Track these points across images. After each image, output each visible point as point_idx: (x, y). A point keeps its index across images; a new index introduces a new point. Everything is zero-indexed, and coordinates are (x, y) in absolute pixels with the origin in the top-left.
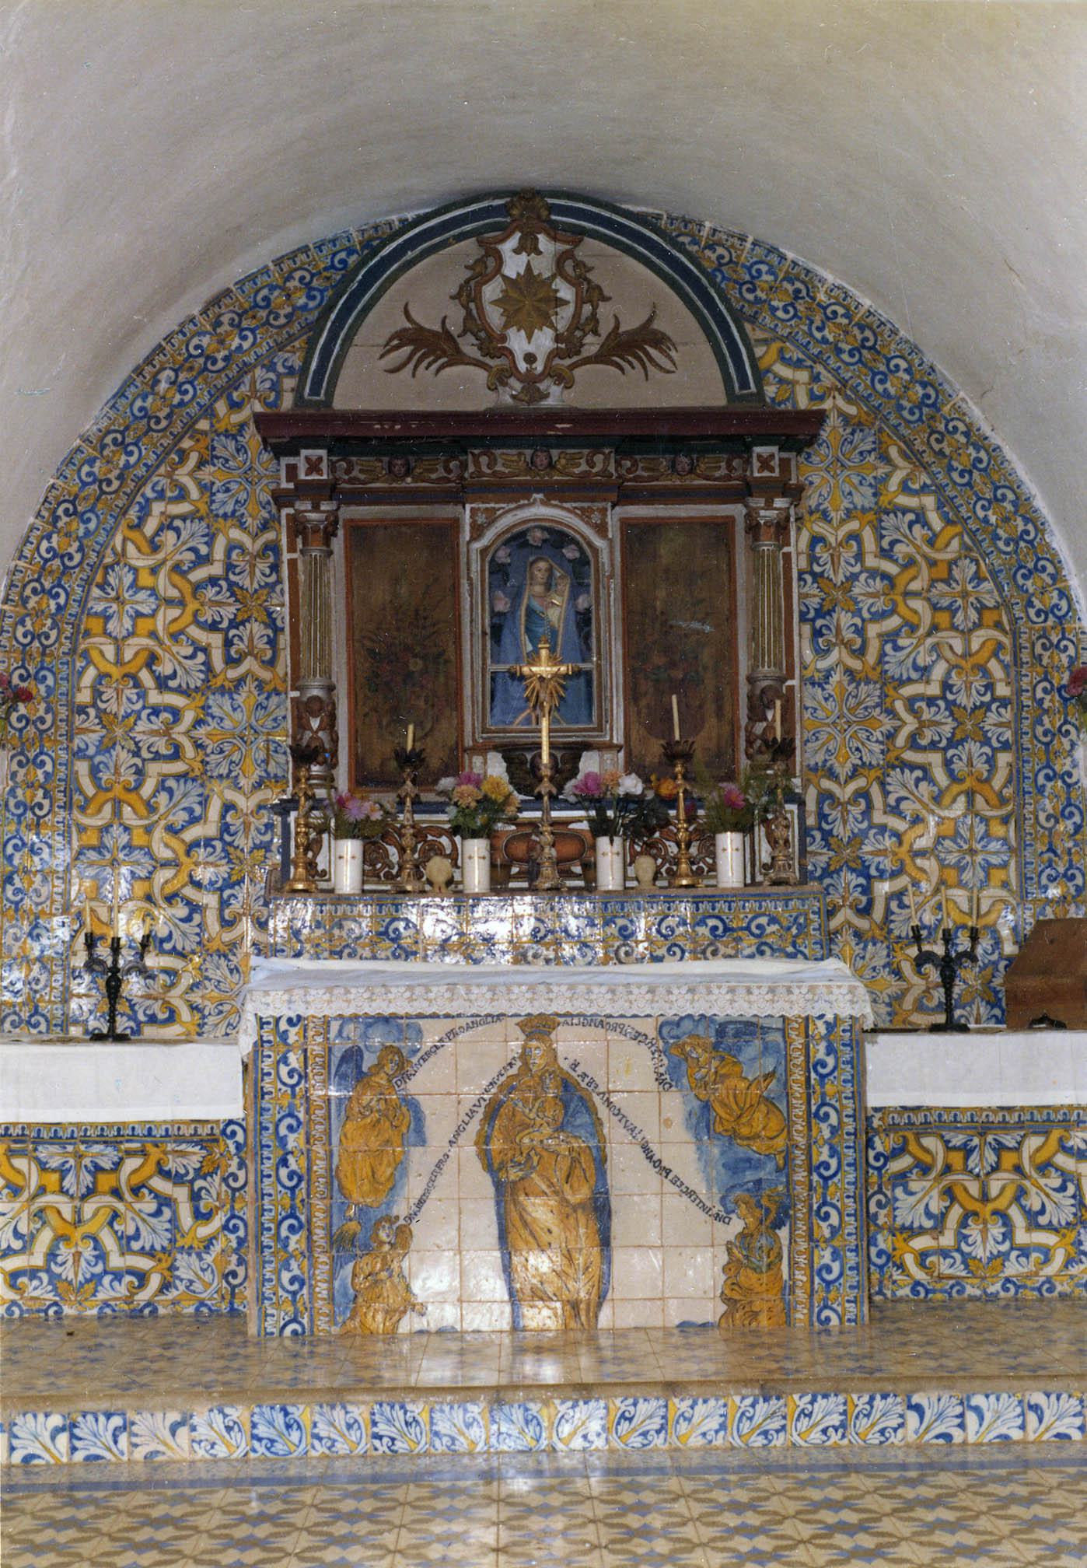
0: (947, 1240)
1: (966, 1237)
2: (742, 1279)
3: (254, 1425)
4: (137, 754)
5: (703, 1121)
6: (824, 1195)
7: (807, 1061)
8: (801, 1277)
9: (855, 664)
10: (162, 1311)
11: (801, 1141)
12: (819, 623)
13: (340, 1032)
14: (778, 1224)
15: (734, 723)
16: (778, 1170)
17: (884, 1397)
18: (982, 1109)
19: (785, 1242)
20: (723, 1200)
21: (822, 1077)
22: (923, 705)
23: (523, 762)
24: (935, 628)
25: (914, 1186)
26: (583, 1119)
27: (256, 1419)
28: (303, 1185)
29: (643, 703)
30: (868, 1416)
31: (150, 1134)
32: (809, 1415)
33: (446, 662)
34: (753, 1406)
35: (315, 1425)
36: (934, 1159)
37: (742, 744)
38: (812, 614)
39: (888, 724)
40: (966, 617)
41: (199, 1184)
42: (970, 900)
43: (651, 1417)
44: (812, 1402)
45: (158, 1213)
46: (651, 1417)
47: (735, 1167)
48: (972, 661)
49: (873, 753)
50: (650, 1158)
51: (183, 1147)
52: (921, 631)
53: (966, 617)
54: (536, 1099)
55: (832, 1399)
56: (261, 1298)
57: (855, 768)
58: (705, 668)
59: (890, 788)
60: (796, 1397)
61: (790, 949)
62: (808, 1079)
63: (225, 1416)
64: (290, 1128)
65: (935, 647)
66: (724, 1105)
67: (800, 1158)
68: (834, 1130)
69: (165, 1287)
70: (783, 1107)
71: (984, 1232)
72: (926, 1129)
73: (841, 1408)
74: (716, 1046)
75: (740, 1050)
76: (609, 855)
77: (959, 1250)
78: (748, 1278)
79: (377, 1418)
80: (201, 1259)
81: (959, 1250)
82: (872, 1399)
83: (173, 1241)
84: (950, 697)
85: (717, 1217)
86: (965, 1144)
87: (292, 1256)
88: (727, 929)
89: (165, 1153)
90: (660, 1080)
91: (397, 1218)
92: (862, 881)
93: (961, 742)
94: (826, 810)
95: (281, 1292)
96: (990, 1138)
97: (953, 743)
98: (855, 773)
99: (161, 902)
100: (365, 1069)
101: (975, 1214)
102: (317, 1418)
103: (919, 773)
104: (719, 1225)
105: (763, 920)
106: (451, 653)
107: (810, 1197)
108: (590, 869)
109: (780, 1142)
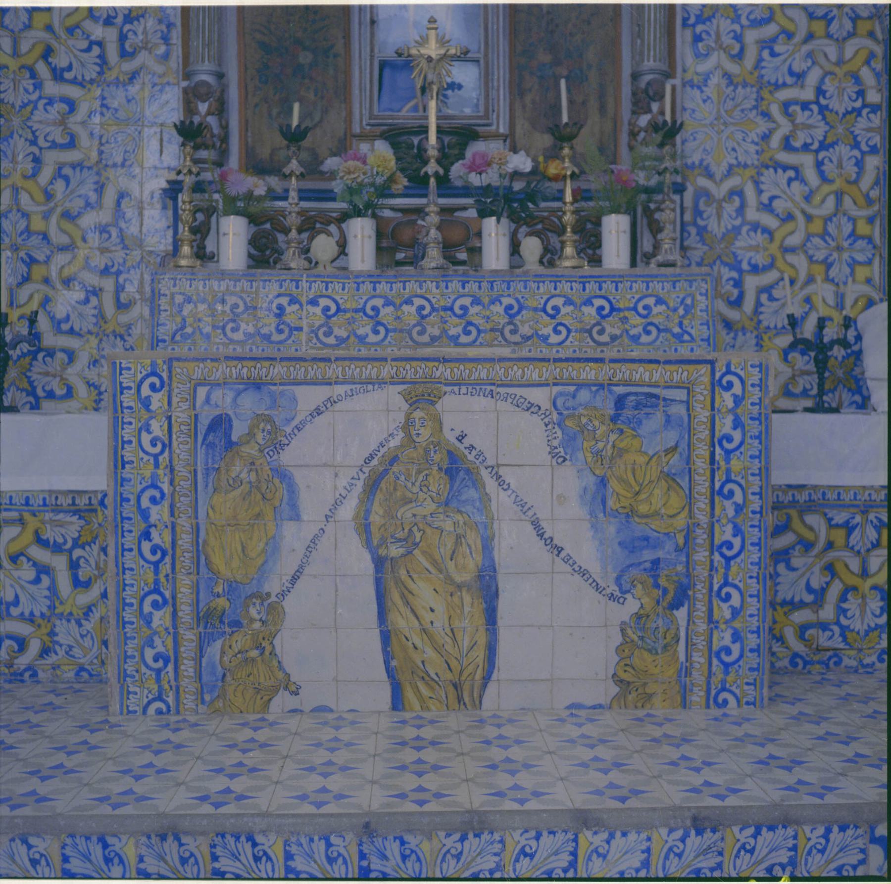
0: (827, 613)
1: (844, 611)
2: (636, 661)
3: (66, 859)
4: (34, 142)
5: (598, 496)
6: (726, 576)
7: (713, 435)
8: (699, 659)
9: (733, 68)
10: (41, 675)
11: (703, 519)
12: (699, 28)
13: (208, 400)
14: (675, 605)
15: (615, 121)
16: (678, 549)
17: (843, 828)
18: (864, 488)
19: (683, 624)
20: (618, 580)
21: (728, 452)
22: (797, 108)
23: (411, 146)
24: (810, 37)
25: (796, 562)
26: (472, 493)
27: (68, 851)
28: (168, 559)
29: (528, 99)
30: (822, 851)
31: (27, 504)
32: (752, 851)
33: (336, 56)
34: (683, 840)
35: (141, 859)
36: (817, 537)
37: (624, 138)
38: (692, 20)
39: (763, 126)
40: (841, 26)
41: (77, 553)
42: (837, 294)
43: (556, 853)
44: (755, 836)
45: (37, 581)
46: (556, 853)
47: (631, 546)
48: (846, 68)
49: (748, 153)
50: (541, 536)
51: (61, 516)
52: (797, 39)
53: (841, 26)
54: (419, 472)
55: (780, 831)
56: (123, 676)
57: (731, 167)
58: (590, 67)
59: (763, 187)
60: (736, 829)
61: (677, 330)
62: (713, 454)
63: (30, 847)
64: (153, 500)
65: (810, 55)
66: (620, 480)
67: (701, 537)
68: (739, 509)
69: (45, 651)
70: (685, 483)
71: (863, 607)
72: (810, 507)
73: (790, 843)
74: (614, 419)
75: (640, 422)
76: (494, 235)
77: (838, 623)
78: (642, 659)
79: (218, 851)
80: (80, 625)
81: (838, 623)
82: (828, 831)
83: (52, 607)
84: (823, 102)
85: (612, 597)
86: (847, 522)
87: (156, 633)
88: (613, 309)
89: (43, 522)
90: (553, 453)
91: (268, 595)
92: (735, 275)
93: (832, 145)
94: (702, 206)
95: (144, 669)
96: (872, 516)
97: (823, 146)
98: (730, 171)
99: (59, 286)
100: (234, 438)
101: (855, 588)
102: (143, 851)
103: (791, 173)
104: (613, 605)
105: (651, 301)
106: (339, 47)
107: (711, 577)
108: (476, 252)
109: (681, 522)
